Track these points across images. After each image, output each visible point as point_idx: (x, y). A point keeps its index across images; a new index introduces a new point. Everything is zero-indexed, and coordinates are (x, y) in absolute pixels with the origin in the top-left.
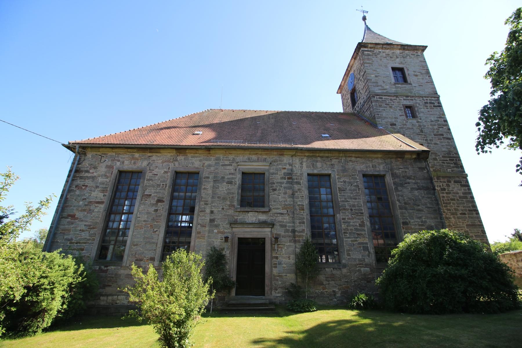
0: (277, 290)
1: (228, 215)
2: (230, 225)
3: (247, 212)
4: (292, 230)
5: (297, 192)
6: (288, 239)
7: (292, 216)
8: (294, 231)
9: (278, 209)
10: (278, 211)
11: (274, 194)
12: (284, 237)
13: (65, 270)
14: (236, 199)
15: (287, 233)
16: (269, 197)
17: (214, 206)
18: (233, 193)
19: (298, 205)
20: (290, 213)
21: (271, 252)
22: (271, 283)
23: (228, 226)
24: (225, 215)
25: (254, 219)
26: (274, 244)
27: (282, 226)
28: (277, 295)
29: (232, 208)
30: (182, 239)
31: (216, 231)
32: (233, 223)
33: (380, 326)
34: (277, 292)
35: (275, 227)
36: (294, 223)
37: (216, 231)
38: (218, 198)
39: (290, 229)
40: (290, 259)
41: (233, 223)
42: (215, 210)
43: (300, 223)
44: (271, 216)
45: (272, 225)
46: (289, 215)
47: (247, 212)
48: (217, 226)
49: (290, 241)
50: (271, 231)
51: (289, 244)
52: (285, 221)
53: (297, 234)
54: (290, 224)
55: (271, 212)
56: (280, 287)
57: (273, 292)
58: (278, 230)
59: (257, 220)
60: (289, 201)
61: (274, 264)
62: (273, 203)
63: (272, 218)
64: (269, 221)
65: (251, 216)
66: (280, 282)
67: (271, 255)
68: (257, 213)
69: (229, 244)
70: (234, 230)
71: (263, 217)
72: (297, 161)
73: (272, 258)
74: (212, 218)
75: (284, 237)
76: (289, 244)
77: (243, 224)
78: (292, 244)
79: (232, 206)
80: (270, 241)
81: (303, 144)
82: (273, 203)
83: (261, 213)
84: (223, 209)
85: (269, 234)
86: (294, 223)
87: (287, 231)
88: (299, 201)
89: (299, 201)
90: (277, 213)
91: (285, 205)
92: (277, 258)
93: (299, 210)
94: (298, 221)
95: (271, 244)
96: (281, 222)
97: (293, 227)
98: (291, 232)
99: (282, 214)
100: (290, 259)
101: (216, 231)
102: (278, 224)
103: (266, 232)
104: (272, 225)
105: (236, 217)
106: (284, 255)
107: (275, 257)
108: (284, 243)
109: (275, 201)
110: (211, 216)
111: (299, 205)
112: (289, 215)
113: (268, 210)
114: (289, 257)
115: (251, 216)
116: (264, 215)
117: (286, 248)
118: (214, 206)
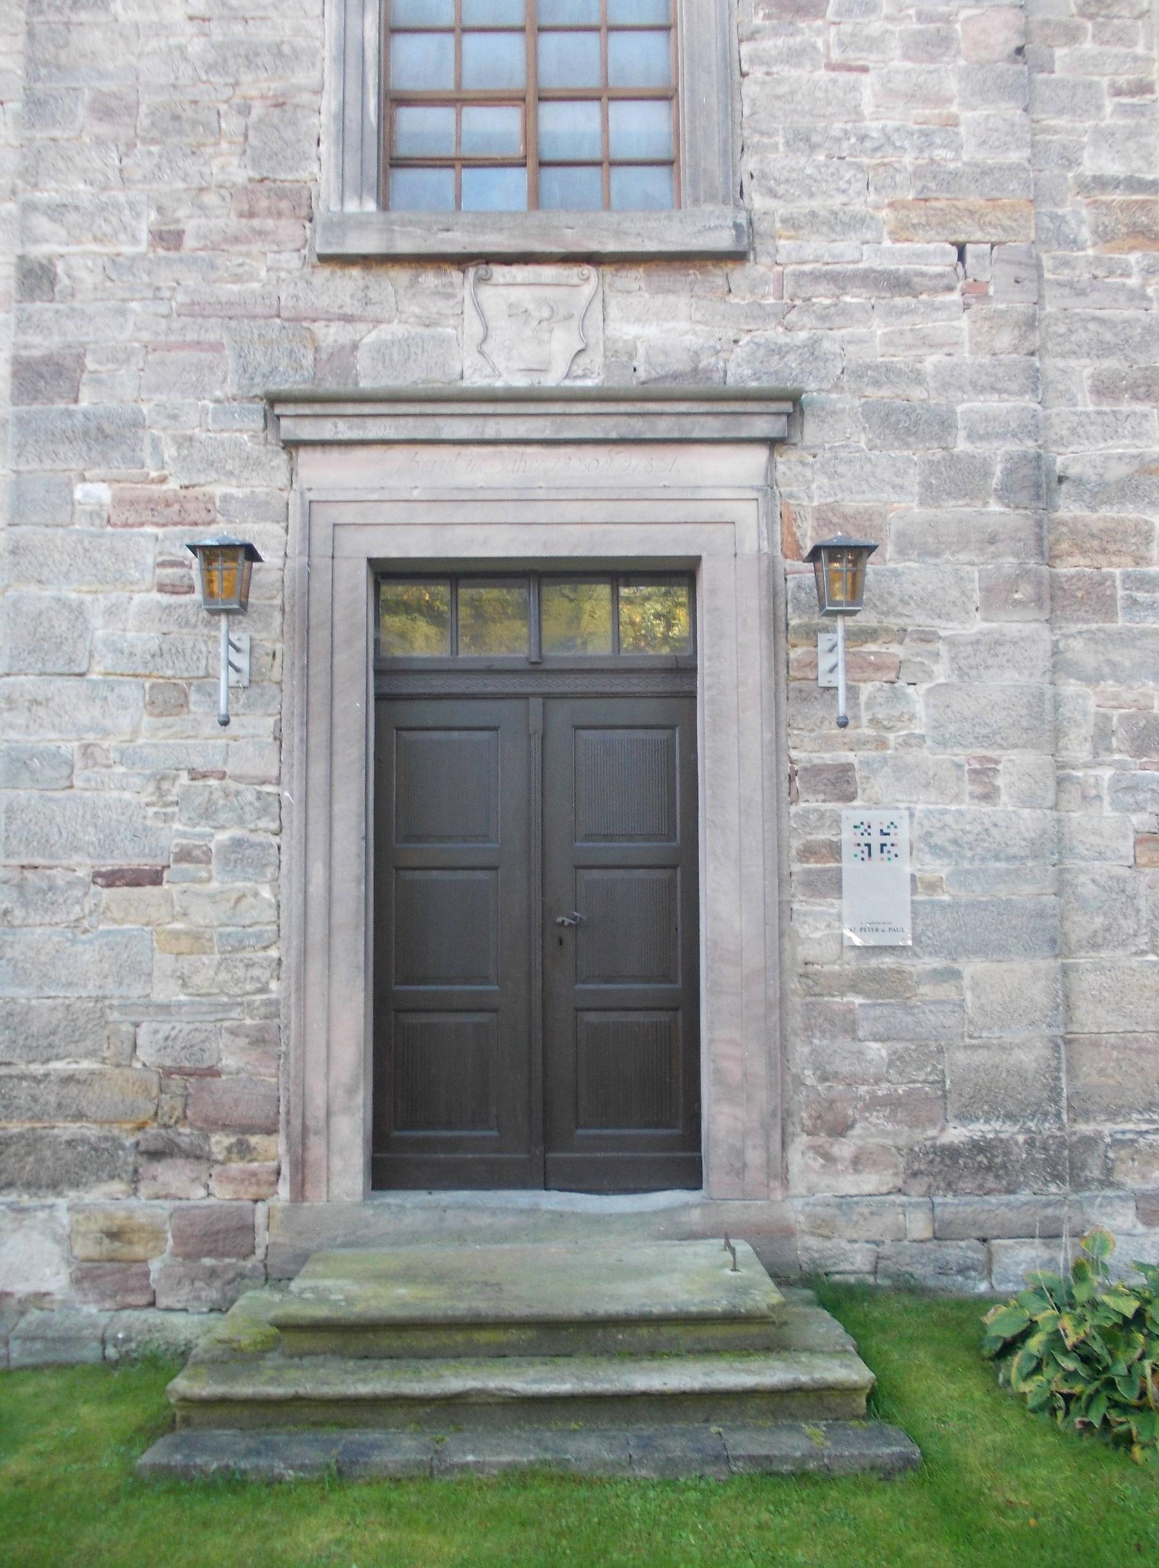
0: (840, 1129)
1: (229, 312)
2: (271, 420)
4: (1014, 465)
5: (1072, 35)
6: (974, 569)
7: (1020, 304)
8: (1038, 483)
9: (839, 223)
10: (850, 252)
11: (794, 56)
12: (925, 545)
14: (324, 123)
15: (953, 510)
16: (730, 92)
17: (57, 211)
18: (283, 56)
19: (1085, 187)
20: (996, 278)
21: (779, 726)
22: (779, 1054)
23: (246, 430)
24: (195, 310)
25: (562, 341)
26: (811, 634)
27: (899, 424)
28: (848, 1184)
31: (95, 493)
32: (298, 410)
34: (844, 1149)
35: (811, 431)
36: (1035, 381)
37: (95, 493)
38: (104, 110)
39: (999, 454)
40: (989, 796)
41: (298, 410)
42: (77, 258)
43: (1105, 389)
44: (758, 314)
45: (779, 414)
46: (977, 291)
47: (462, 261)
48: (107, 437)
49: (997, 596)
50: (770, 485)
51: (977, 625)
52: (932, 361)
53: (1069, 510)
54: (993, 404)
55: (759, 267)
56: (874, 1104)
57: (799, 1158)
58: (847, 477)
59: (595, 360)
60: (980, 130)
61: (808, 852)
62: (780, 161)
63: (775, 334)
65: (516, 312)
66: (877, 1051)
67: (777, 747)
69: (267, 632)
70: (317, 470)
72: (922, 1355)
73: (789, 780)
74: (40, 345)
75: (925, 545)
76: (977, 625)
77: (433, 408)
78: (1017, 625)
79: (272, 198)
80: (753, 601)
81: (485, 1138)
83: (633, 277)
84: (168, 238)
85: (747, 513)
86: (1035, 381)
87: (956, 479)
88: (1104, 136)
89: (1104, 136)
90: (839, 280)
91: (934, 178)
92: (840, 783)
93: (1104, 236)
94: (1085, 369)
95: (777, 627)
96: (886, 374)
97: (1034, 427)
98: (1005, 493)
99: (899, 284)
100: (989, 796)
101: (103, 493)
102: (845, 401)
103: (705, 498)
104: (779, 414)
105: (331, 335)
106: (925, 755)
107: (815, 771)
108: (921, 620)
109: (803, 140)
110: (24, 323)
111: (1102, 183)
112: (977, 291)
113: (723, 241)
114: (984, 773)
115: (516, 312)
116: (681, 302)
117: (941, 672)
118: (57, 211)
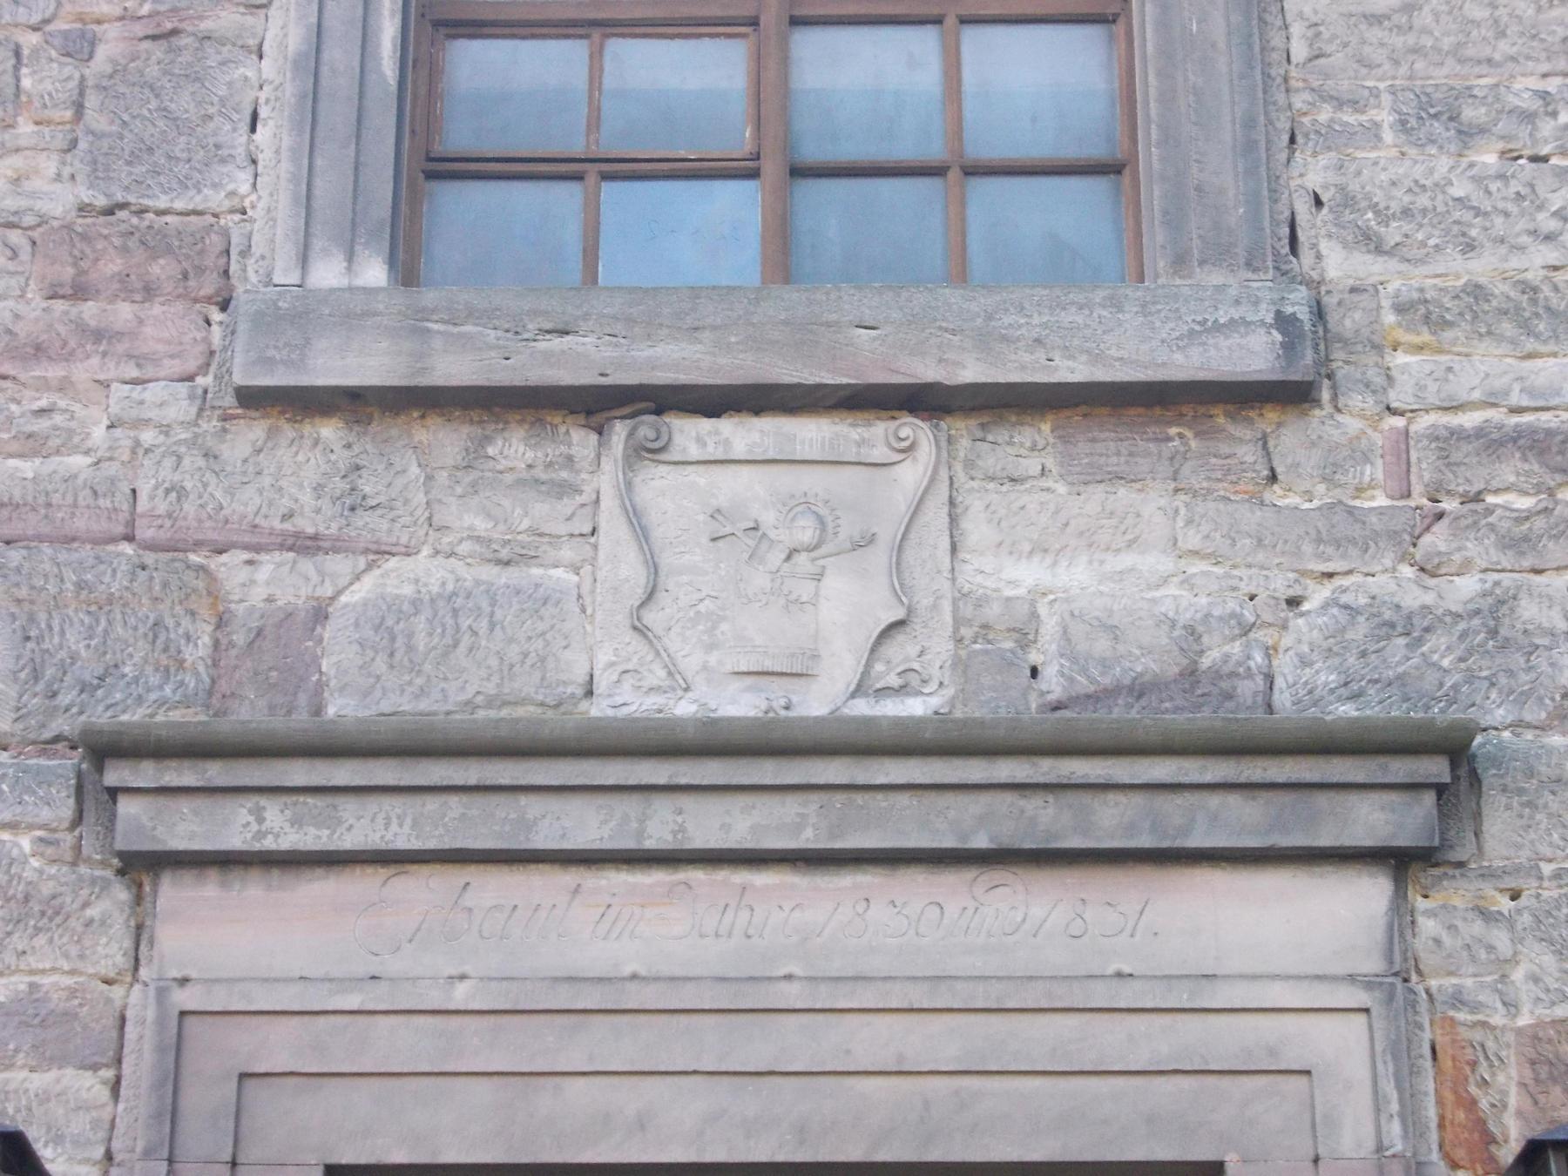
2: (94, 799)
3: (596, 405)
13: (209, 593)
14: (270, 76)
25: (847, 604)
29: (167, 326)
30: (1156, 237)
33: (75, 450)
35: (1501, 830)
44: (1345, 531)
47: (596, 405)
50: (1399, 977)
55: (1345, 421)
59: (932, 647)
62: (1386, 166)
63: (1397, 585)
64: (1304, 676)
65: (731, 531)
68: (912, 456)
70: (219, 938)
71: (1096, 571)
77: (513, 773)
82: (1386, 166)
83: (1028, 447)
85: (1344, 1047)
105: (260, 584)
109: (1439, 117)
113: (1253, 355)
115: (731, 531)
